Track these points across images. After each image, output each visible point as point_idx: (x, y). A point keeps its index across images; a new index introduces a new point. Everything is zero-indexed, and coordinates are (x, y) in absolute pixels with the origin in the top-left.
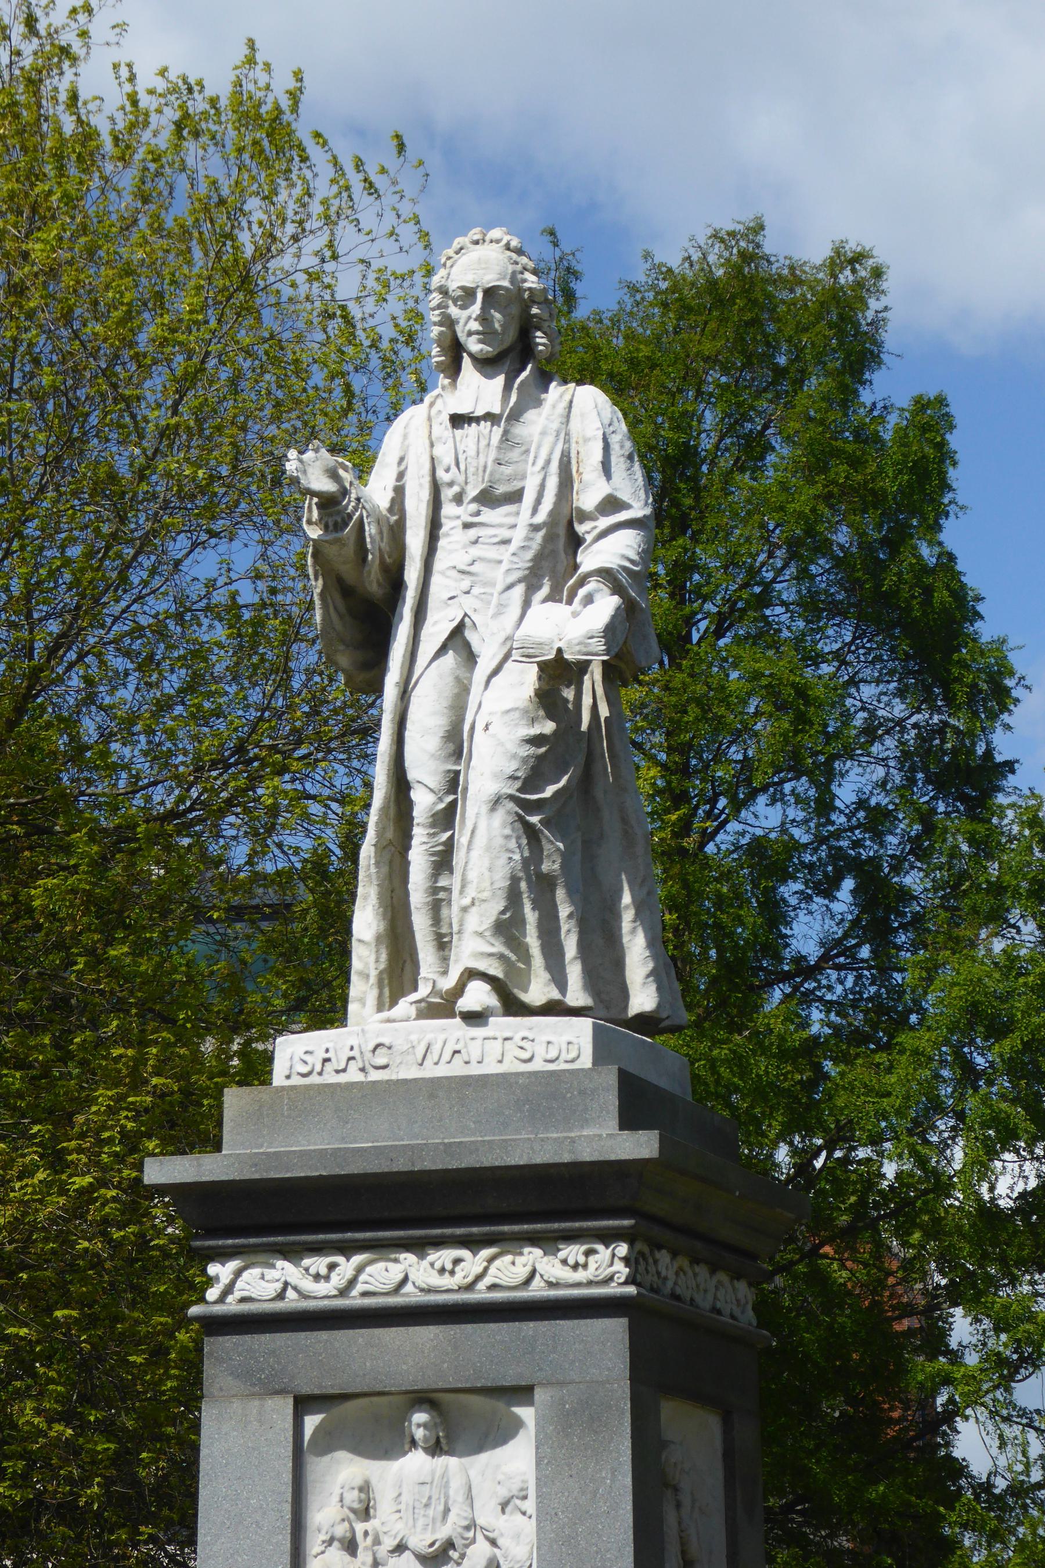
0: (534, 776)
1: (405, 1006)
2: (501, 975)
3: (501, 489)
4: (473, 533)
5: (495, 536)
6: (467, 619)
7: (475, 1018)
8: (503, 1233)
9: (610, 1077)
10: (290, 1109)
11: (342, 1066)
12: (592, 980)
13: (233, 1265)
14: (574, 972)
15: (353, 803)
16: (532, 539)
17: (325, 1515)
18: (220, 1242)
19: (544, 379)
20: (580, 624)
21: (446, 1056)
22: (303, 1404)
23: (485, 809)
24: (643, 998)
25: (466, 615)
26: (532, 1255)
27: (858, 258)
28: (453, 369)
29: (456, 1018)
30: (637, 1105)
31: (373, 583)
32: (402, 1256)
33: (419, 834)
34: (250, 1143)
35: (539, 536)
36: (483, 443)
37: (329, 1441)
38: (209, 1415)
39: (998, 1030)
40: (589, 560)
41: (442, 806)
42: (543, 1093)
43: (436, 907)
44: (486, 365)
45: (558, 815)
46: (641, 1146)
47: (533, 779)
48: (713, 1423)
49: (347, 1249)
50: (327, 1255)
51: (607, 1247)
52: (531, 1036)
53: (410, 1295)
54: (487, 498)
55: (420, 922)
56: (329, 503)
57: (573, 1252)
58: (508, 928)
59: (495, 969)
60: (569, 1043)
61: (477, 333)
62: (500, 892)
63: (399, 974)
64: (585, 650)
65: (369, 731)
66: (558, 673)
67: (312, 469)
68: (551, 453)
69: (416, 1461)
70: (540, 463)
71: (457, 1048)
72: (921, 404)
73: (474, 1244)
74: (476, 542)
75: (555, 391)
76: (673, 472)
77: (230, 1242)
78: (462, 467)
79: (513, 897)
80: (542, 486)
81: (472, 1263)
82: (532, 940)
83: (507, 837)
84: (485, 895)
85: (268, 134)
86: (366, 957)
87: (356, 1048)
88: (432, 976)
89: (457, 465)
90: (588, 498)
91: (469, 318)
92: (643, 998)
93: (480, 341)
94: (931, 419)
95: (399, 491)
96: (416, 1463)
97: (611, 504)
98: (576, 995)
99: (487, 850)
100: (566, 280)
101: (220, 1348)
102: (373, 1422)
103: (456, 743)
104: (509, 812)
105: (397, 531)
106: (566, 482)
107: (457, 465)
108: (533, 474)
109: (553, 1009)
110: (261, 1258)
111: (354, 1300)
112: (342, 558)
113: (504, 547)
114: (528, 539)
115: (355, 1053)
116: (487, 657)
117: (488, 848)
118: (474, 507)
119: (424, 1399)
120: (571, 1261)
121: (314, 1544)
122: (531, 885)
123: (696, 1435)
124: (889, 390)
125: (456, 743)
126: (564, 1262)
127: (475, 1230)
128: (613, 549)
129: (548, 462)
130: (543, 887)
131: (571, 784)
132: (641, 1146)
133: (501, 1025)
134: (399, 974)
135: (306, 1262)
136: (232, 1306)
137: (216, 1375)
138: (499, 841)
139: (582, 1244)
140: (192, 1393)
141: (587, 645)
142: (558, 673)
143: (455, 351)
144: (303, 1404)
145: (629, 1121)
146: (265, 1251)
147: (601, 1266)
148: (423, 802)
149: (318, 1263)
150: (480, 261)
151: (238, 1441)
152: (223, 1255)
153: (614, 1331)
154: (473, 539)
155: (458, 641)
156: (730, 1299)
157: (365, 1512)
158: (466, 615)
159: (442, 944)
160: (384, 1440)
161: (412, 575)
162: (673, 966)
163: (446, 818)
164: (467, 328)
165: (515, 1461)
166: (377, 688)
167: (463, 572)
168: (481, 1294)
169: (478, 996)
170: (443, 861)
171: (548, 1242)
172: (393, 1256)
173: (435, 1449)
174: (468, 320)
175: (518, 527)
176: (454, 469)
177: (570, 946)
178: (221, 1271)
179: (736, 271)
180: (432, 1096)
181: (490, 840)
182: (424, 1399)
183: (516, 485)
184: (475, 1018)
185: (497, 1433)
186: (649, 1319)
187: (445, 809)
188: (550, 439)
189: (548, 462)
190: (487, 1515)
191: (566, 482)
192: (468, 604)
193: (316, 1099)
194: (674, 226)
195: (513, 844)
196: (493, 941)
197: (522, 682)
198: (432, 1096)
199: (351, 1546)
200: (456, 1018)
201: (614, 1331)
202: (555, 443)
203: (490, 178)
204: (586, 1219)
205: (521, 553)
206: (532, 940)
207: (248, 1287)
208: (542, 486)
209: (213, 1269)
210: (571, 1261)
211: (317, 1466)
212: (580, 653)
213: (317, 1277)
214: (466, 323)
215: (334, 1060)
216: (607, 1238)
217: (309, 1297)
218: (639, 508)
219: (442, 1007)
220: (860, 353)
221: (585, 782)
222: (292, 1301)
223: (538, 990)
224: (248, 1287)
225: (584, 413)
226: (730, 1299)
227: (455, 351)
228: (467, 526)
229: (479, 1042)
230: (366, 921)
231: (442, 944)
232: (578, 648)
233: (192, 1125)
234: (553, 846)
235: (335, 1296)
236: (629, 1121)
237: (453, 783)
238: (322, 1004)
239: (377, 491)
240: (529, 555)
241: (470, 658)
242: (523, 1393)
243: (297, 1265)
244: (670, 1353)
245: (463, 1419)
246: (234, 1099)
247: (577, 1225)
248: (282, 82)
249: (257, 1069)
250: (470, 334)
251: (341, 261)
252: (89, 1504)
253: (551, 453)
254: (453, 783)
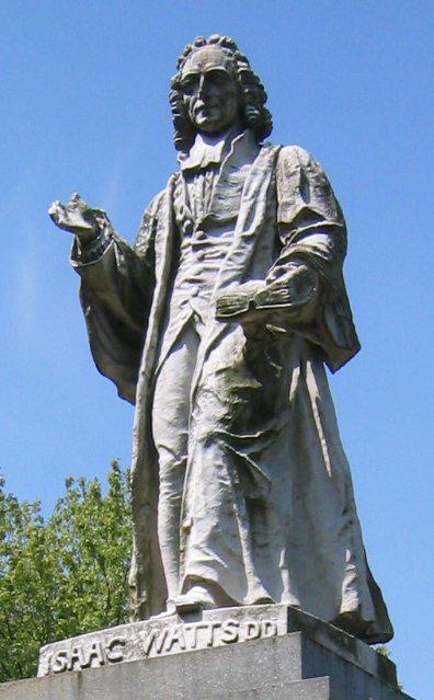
2: (215, 579)
3: (222, 217)
5: (217, 252)
6: (196, 316)
11: (87, 662)
16: (243, 248)
21: (167, 646)
23: (200, 446)
25: (195, 312)
33: (164, 486)
35: (250, 247)
36: (208, 185)
41: (178, 463)
52: (236, 622)
59: (210, 574)
62: (213, 512)
68: (260, 186)
70: (251, 193)
71: (176, 637)
78: (192, 206)
80: (252, 209)
83: (220, 467)
87: (98, 647)
89: (189, 204)
95: (152, 243)
104: (221, 448)
107: (189, 204)
108: (245, 201)
114: (241, 247)
115: (97, 651)
117: (203, 475)
118: (201, 233)
129: (257, 193)
138: (212, 470)
155: (191, 337)
158: (195, 312)
159: (178, 554)
176: (186, 208)
181: (204, 470)
183: (234, 213)
187: (180, 465)
188: (260, 177)
189: (257, 193)
192: (195, 304)
195: (224, 472)
196: (208, 551)
202: (263, 180)
205: (236, 258)
208: (252, 209)
214: (194, 103)
215: (80, 658)
229: (193, 631)
240: (242, 259)
252: (251, 114)
253: (260, 186)
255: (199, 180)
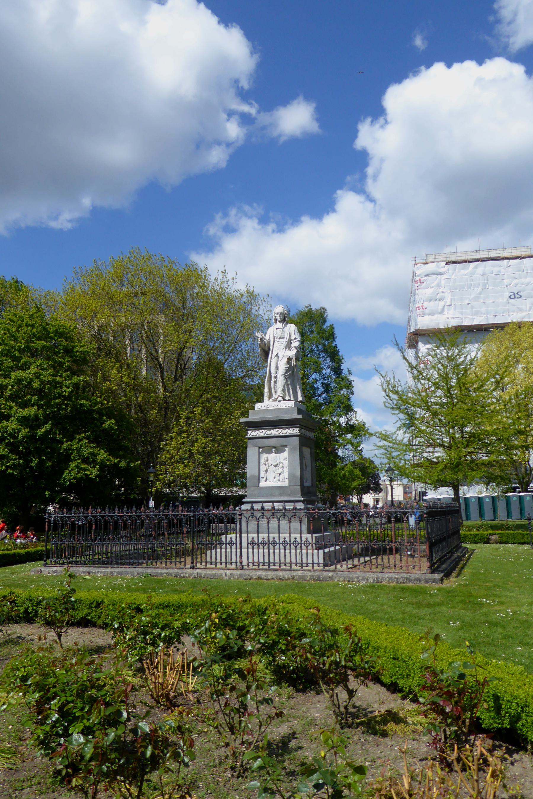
0: (287, 372)
1: (271, 400)
7: (280, 401)
9: (296, 408)
12: (294, 397)
14: (292, 396)
15: (263, 378)
17: (262, 461)
19: (287, 323)
20: (292, 353)
22: (260, 448)
24: (300, 399)
26: (287, 430)
27: (324, 308)
28: (276, 322)
29: (278, 401)
30: (300, 412)
31: (267, 349)
33: (273, 379)
34: (253, 417)
37: (262, 452)
38: (248, 449)
39: (342, 403)
40: (293, 345)
42: (288, 410)
43: (275, 388)
44: (280, 322)
45: (289, 376)
46: (300, 416)
47: (286, 372)
48: (309, 449)
49: (264, 429)
53: (272, 435)
54: (280, 338)
55: (273, 390)
56: (261, 339)
57: (292, 429)
58: (283, 390)
60: (291, 404)
63: (270, 396)
65: (266, 367)
66: (289, 359)
67: (259, 335)
69: (273, 454)
72: (330, 325)
73: (280, 428)
75: (289, 325)
76: (302, 334)
79: (284, 387)
81: (280, 431)
82: (287, 392)
85: (252, 296)
86: (266, 394)
88: (274, 396)
90: (293, 338)
92: (300, 399)
94: (332, 327)
96: (273, 455)
97: (295, 339)
98: (292, 399)
99: (281, 381)
100: (289, 313)
101: (250, 442)
102: (268, 450)
103: (277, 368)
105: (269, 342)
106: (290, 336)
109: (289, 400)
111: (266, 435)
112: (263, 346)
113: (283, 344)
116: (281, 357)
119: (274, 447)
121: (261, 464)
122: (286, 385)
123: (307, 451)
124: (327, 324)
125: (277, 368)
128: (296, 344)
130: (288, 385)
131: (291, 373)
132: (300, 416)
133: (283, 402)
134: (270, 396)
136: (251, 436)
137: (249, 445)
140: (246, 447)
142: (289, 359)
143: (276, 320)
144: (260, 448)
145: (299, 413)
147: (295, 431)
148: (273, 375)
149: (261, 431)
150: (279, 309)
151: (252, 452)
153: (297, 438)
156: (311, 435)
157: (267, 461)
159: (276, 392)
160: (270, 452)
161: (271, 348)
162: (303, 395)
163: (276, 377)
165: (285, 454)
166: (267, 361)
168: (281, 435)
169: (280, 399)
170: (275, 382)
171: (289, 428)
173: (276, 453)
174: (278, 316)
175: (284, 342)
177: (291, 393)
179: (309, 311)
182: (274, 447)
184: (280, 401)
185: (284, 451)
186: (301, 437)
190: (282, 461)
191: (290, 336)
193: (260, 411)
194: (302, 305)
197: (285, 360)
199: (265, 465)
200: (278, 401)
201: (297, 438)
203: (280, 300)
206: (287, 392)
211: (261, 455)
216: (296, 428)
218: (299, 339)
219: (275, 400)
220: (325, 320)
221: (293, 372)
222: (258, 436)
223: (287, 398)
225: (292, 328)
226: (311, 435)
227: (276, 320)
230: (266, 390)
231: (276, 392)
233: (245, 414)
234: (289, 380)
236: (299, 413)
237: (277, 373)
238: (260, 399)
239: (267, 338)
241: (278, 357)
242: (286, 446)
244: (304, 441)
245: (279, 449)
246: (251, 412)
248: (252, 289)
249: (253, 408)
251: (262, 310)
254: (277, 373)
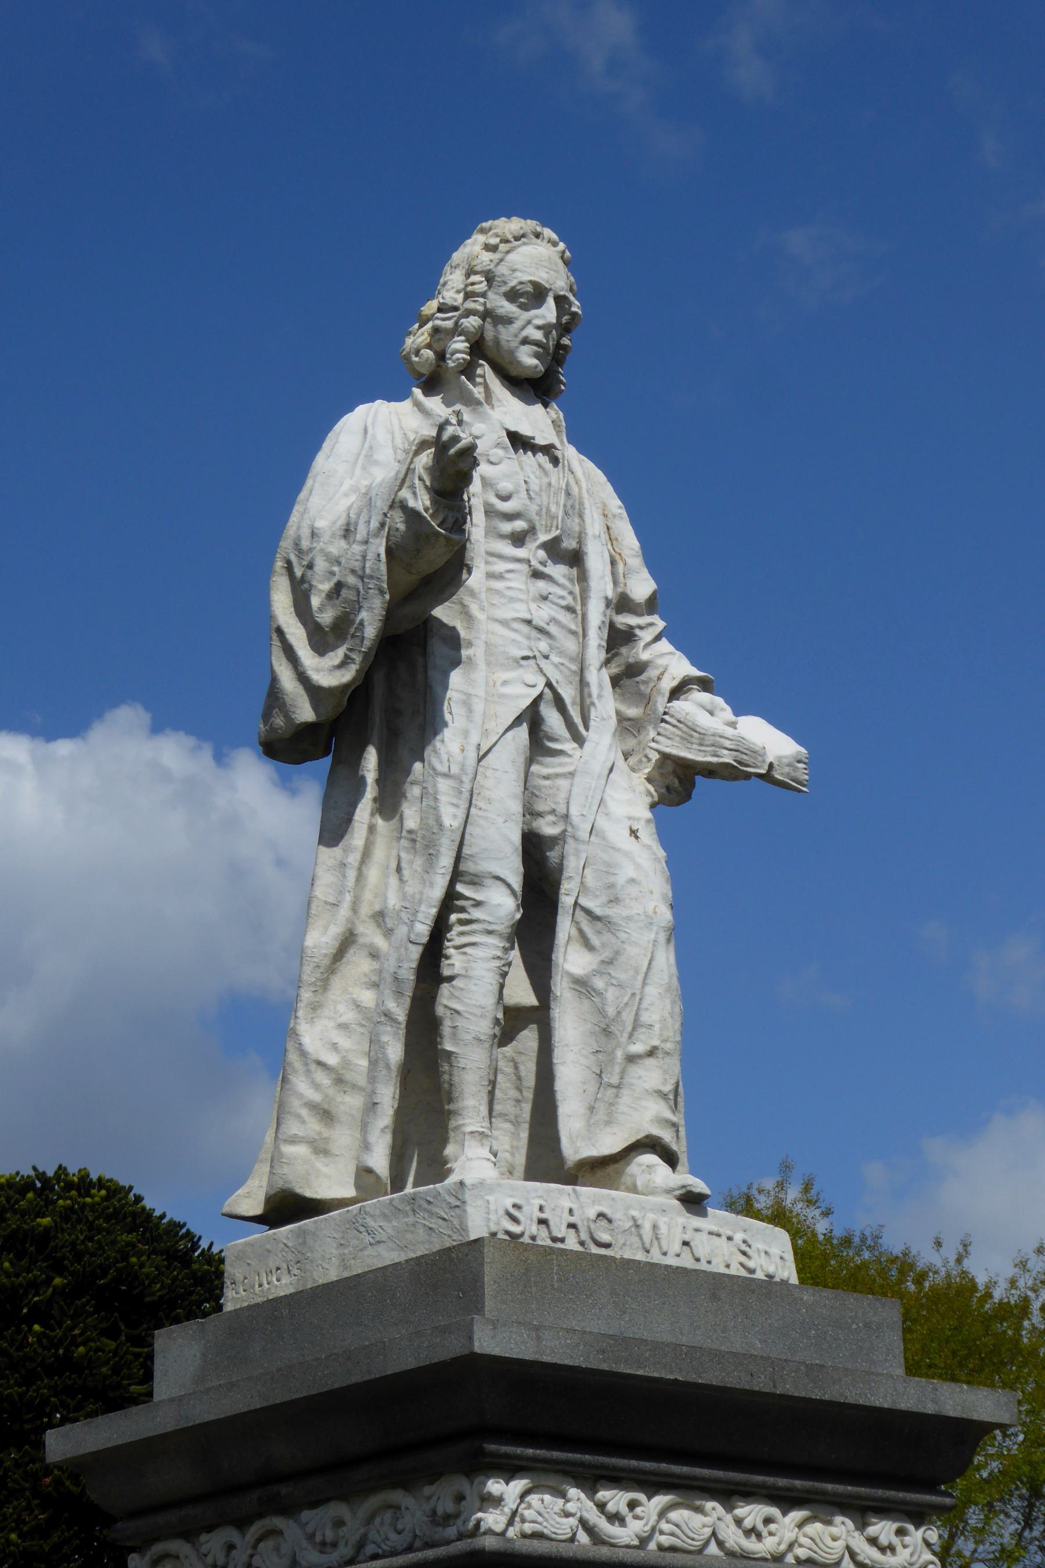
4: (541, 585)
8: (824, 1493)
10: (560, 1280)
13: (519, 1485)
18: (519, 1451)
32: (710, 1505)
50: (627, 1489)
51: (917, 1528)
61: (537, 343)
64: (793, 774)
73: (787, 1501)
74: (545, 598)
77: (530, 1451)
84: (669, 1046)
91: (529, 322)
93: (537, 356)
110: (552, 1480)
120: (611, 1507)
126: (739, 1522)
127: (798, 1483)
135: (603, 1495)
139: (894, 1521)
141: (796, 769)
146: (557, 1472)
152: (510, 1470)
154: (545, 593)
164: (524, 333)
167: (541, 630)
172: (698, 1503)
178: (508, 1489)
180: (714, 1297)
198: (714, 1297)
204: (609, 1455)
207: (540, 1519)
209: (495, 1486)
210: (748, 1523)
212: (788, 775)
213: (752, 1532)
214: (523, 328)
217: (604, 1543)
224: (540, 1519)
228: (537, 575)
232: (787, 770)
235: (635, 1547)
243: (729, 1509)
247: (901, 1495)
250: (525, 341)
255: (528, 459)
